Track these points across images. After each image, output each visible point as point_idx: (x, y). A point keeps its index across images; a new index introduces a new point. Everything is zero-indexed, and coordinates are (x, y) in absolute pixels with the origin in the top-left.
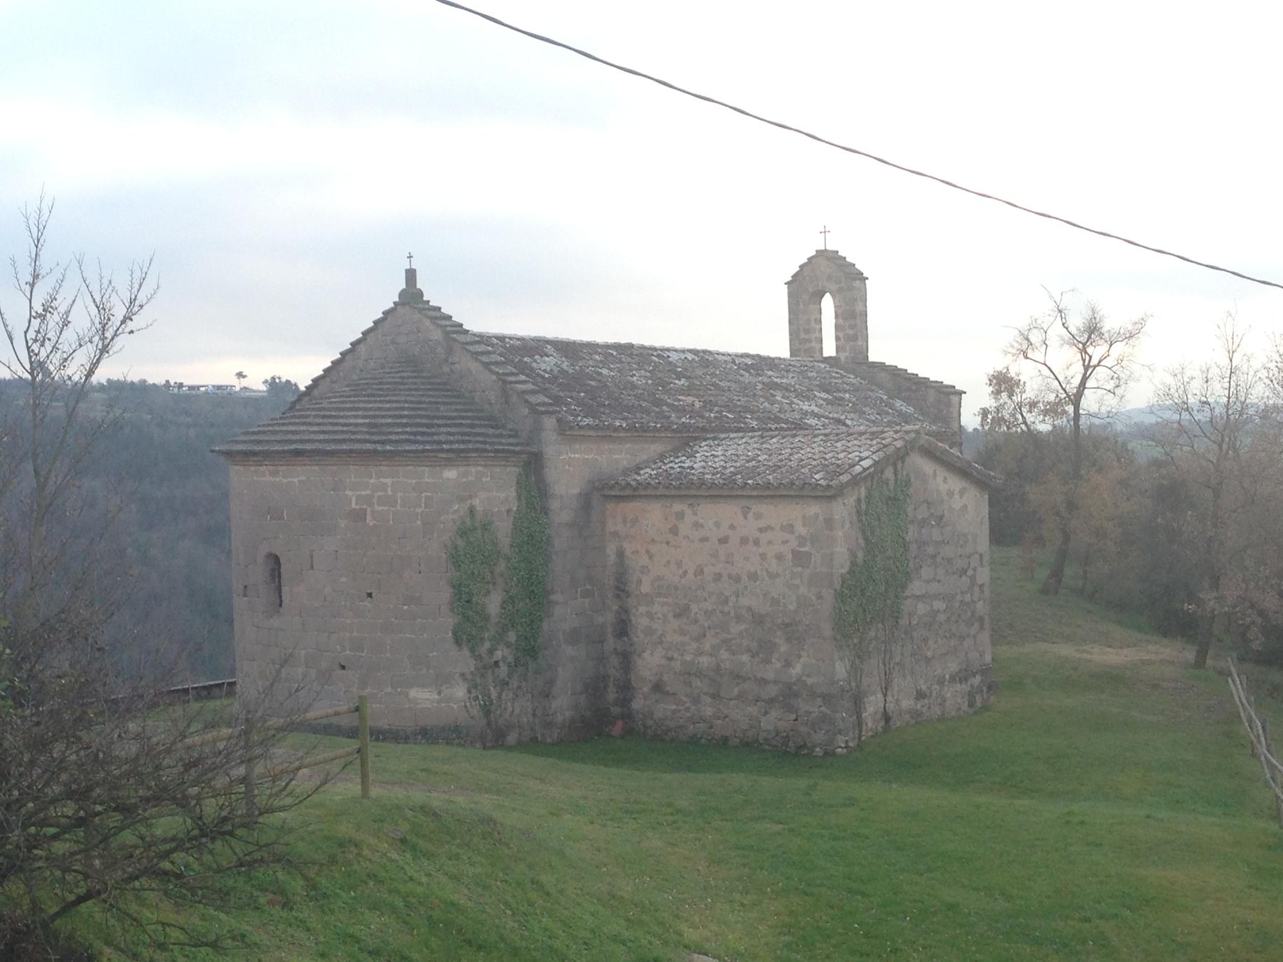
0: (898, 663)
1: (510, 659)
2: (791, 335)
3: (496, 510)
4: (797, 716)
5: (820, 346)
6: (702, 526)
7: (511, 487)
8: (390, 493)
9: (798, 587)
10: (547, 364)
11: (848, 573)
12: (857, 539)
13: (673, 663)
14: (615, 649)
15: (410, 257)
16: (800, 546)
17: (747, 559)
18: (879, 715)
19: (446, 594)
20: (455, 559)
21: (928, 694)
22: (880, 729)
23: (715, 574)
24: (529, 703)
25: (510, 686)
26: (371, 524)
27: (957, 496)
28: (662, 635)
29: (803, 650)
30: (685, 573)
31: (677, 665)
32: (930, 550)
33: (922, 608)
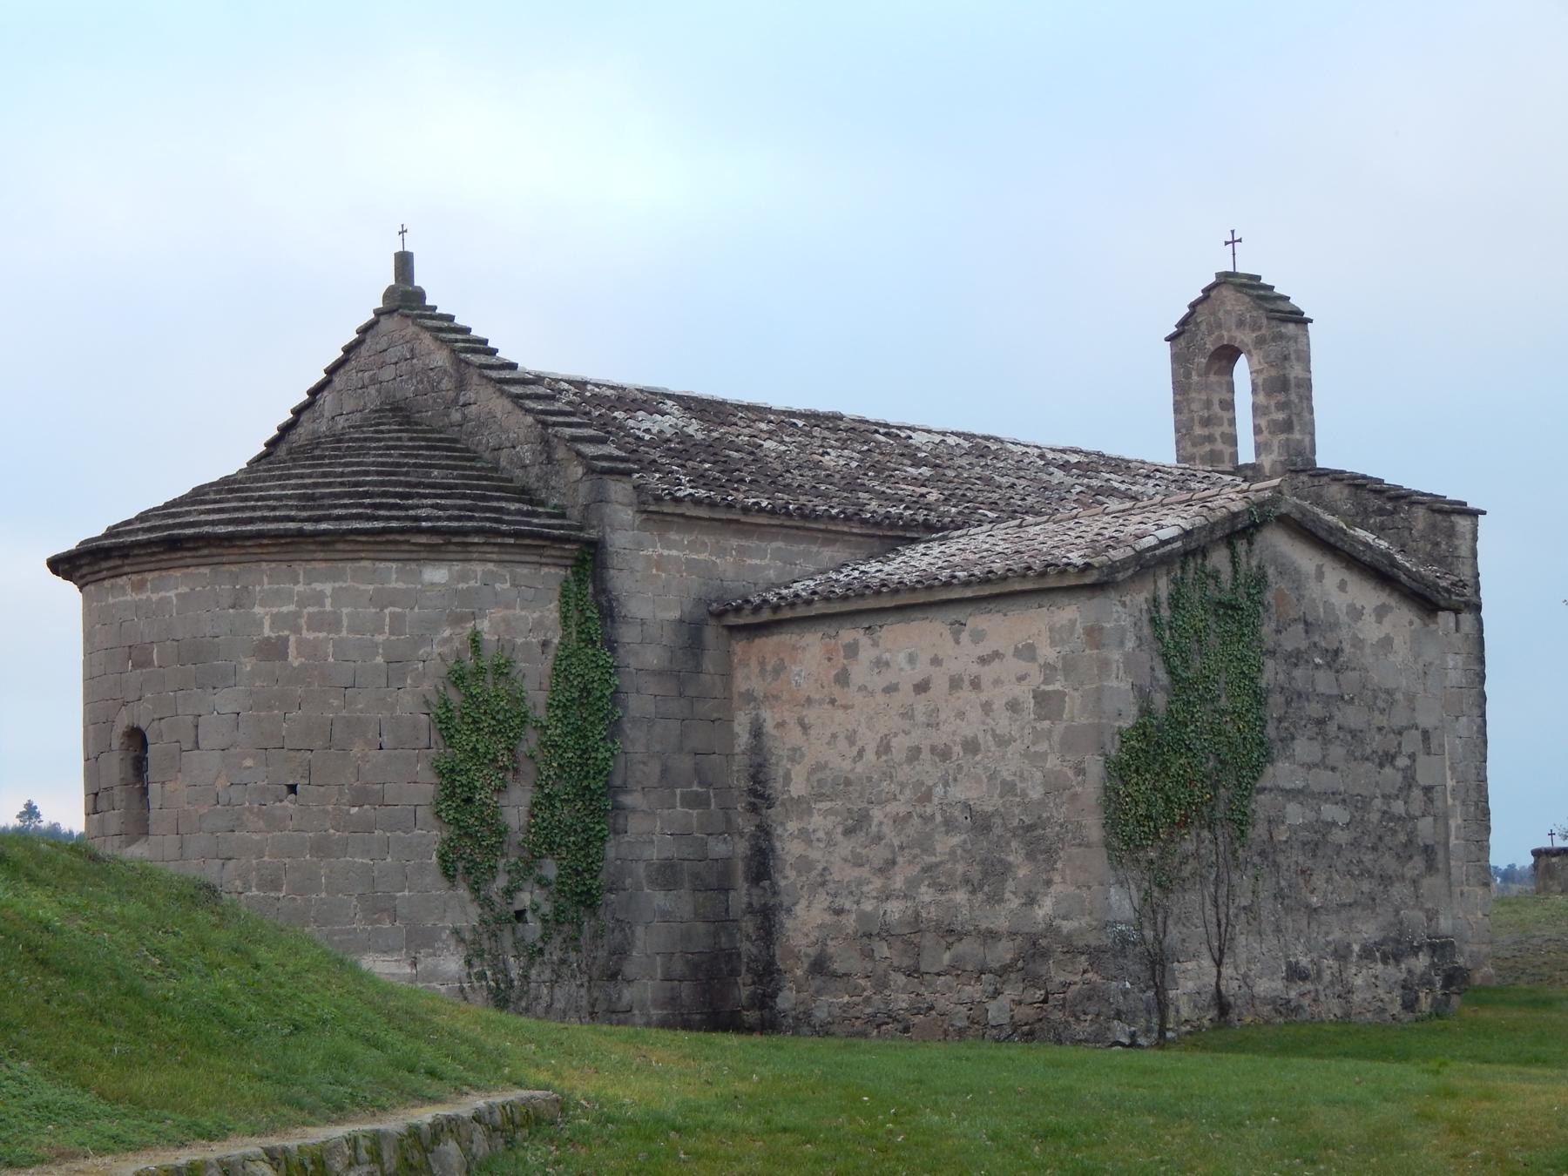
0: (1244, 908)
1: (547, 908)
2: (1177, 431)
3: (519, 641)
4: (1047, 993)
5: (1230, 450)
6: (887, 664)
7: (551, 602)
8: (328, 608)
9: (1044, 756)
10: (666, 423)
11: (1134, 728)
12: (1152, 669)
13: (843, 919)
14: (750, 905)
15: (403, 232)
16: (1046, 682)
17: (961, 715)
18: (1206, 998)
19: (427, 788)
20: (445, 726)
21: (1313, 974)
22: (1206, 1022)
23: (910, 749)
24: (583, 991)
25: (547, 957)
26: (296, 664)
27: (1369, 617)
28: (825, 869)
29: (1054, 869)
30: (861, 753)
31: (850, 922)
32: (1315, 709)
33: (1296, 814)
